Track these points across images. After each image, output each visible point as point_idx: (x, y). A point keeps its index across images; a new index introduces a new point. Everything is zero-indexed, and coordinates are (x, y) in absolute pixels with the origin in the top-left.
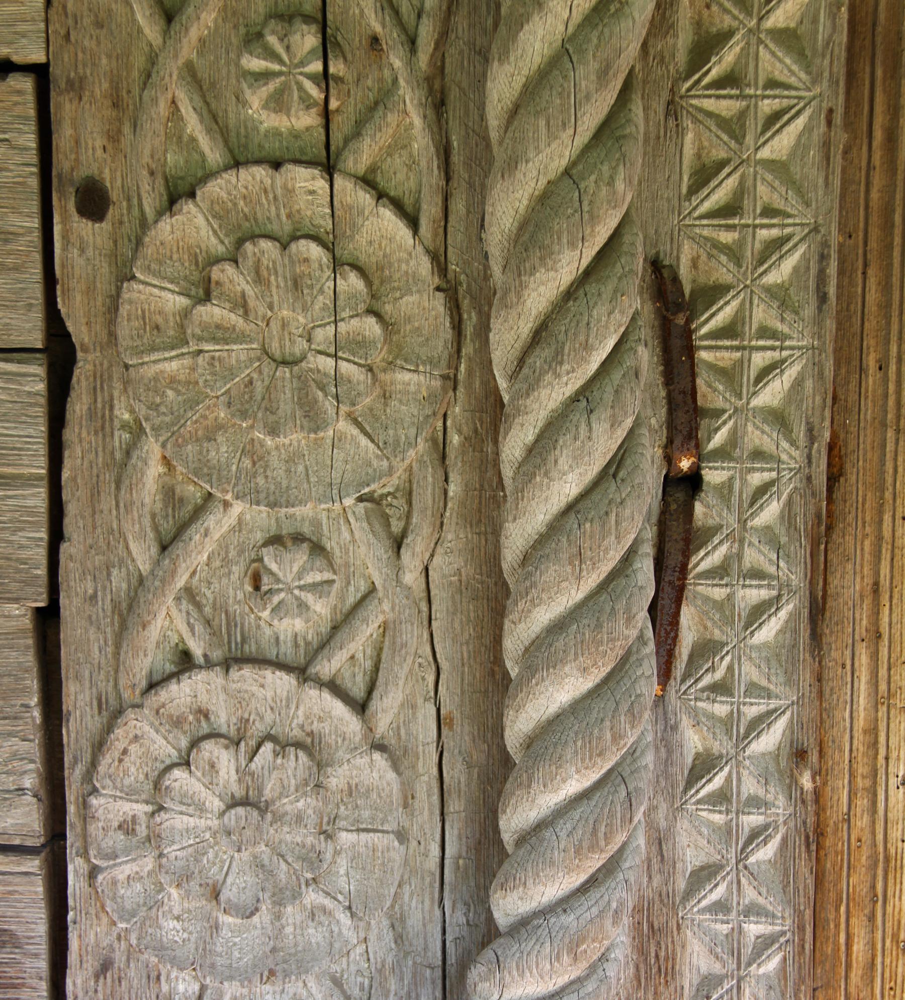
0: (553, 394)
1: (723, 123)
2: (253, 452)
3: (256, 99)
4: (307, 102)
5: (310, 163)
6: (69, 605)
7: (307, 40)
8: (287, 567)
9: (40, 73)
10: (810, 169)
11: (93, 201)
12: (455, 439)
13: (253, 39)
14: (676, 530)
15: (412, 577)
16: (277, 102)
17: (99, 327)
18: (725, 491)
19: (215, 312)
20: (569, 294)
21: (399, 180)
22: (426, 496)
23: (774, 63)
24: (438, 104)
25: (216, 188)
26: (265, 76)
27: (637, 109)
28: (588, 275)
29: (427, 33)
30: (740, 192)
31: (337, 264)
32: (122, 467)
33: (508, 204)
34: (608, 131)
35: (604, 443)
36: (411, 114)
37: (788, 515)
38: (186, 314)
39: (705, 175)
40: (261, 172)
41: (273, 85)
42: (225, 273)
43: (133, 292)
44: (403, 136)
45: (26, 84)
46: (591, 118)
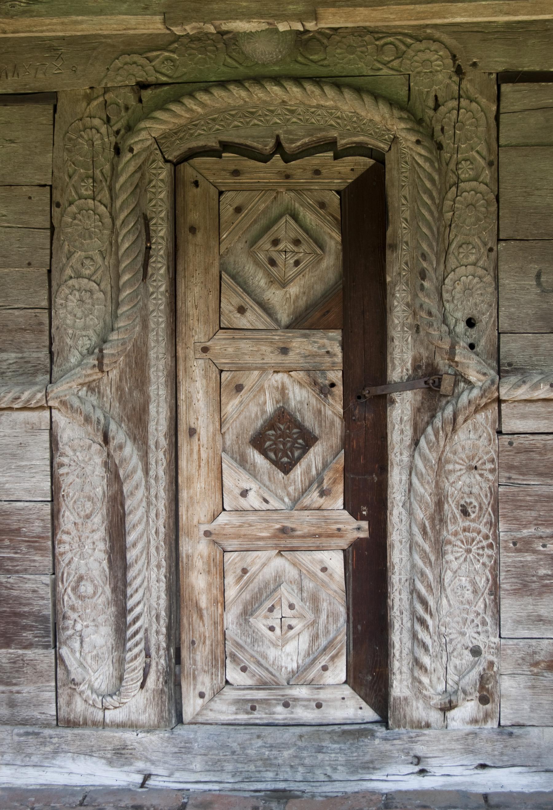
1: (153, 193)
2: (82, 244)
4: (90, 189)
7: (91, 181)
8: (87, 262)
10: (165, 200)
11: (58, 205)
13: (83, 181)
16: (86, 190)
18: (154, 249)
19: (76, 222)
20: (127, 216)
22: (109, 250)
23: (160, 184)
25: (77, 203)
29: (108, 180)
31: (95, 214)
32: (62, 246)
37: (164, 253)
39: (151, 200)
40: (83, 200)
43: (64, 219)
45: (48, 188)
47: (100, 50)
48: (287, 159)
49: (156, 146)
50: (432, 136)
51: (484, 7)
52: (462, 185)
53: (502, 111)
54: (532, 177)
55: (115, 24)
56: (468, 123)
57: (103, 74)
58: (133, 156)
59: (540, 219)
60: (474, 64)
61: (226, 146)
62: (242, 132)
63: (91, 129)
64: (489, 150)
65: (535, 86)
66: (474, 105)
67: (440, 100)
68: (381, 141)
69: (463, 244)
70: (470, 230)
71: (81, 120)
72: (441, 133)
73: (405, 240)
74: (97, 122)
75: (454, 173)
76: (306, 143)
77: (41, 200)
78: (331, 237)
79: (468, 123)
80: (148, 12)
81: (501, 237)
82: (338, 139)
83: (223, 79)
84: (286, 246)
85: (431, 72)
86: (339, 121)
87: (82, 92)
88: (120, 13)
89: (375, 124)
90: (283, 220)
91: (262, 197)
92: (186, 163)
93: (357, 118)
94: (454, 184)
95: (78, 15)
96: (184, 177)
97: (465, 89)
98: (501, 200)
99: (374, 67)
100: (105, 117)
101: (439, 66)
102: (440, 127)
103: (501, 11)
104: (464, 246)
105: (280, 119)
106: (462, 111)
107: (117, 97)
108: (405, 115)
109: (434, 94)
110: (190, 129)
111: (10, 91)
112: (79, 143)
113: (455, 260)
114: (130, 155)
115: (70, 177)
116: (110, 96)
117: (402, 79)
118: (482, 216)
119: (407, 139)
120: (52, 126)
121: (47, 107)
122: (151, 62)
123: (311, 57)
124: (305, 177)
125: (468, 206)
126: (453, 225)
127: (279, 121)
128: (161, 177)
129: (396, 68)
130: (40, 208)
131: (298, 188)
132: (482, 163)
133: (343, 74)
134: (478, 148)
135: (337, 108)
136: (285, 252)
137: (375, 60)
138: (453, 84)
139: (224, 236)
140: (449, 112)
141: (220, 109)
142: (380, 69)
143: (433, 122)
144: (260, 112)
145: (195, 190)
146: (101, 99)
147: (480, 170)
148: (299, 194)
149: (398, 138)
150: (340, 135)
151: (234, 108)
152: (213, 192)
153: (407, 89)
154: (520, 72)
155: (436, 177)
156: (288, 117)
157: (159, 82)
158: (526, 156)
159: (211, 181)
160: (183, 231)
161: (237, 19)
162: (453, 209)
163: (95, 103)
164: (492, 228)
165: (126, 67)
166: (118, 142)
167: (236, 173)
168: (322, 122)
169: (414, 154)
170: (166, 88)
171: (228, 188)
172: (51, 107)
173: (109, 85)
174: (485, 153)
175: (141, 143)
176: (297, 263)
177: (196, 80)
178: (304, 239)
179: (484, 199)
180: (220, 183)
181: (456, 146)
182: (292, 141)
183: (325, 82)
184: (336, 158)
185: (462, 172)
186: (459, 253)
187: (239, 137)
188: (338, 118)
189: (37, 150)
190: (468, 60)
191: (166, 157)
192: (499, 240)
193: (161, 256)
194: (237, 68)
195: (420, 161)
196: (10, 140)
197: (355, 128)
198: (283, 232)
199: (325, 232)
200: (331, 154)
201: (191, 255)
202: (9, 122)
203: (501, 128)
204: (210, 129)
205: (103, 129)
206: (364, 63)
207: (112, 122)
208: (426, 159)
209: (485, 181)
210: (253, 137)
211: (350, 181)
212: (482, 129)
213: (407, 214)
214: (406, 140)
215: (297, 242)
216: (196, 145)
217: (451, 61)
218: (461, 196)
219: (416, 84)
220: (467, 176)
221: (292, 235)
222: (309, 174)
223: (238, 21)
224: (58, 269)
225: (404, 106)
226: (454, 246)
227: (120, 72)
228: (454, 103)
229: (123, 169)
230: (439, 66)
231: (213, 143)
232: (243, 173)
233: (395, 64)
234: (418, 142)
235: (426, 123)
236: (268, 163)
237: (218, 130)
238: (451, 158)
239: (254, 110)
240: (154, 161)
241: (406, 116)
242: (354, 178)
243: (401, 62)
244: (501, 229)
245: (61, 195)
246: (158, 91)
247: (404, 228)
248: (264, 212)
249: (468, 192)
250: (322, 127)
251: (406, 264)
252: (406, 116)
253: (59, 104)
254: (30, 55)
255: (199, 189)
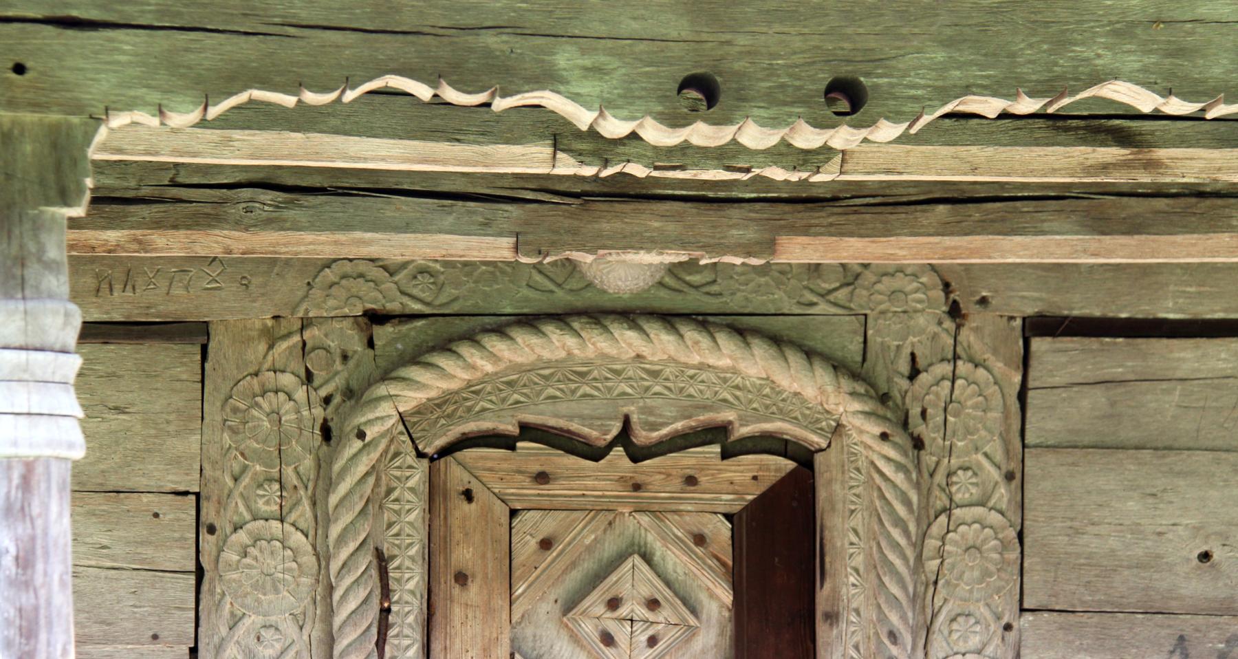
0: (348, 581)
1: (395, 511)
2: (258, 600)
3: (261, 502)
4: (276, 503)
6: (201, 646)
7: (276, 486)
8: (267, 635)
9: (198, 495)
10: (419, 524)
11: (212, 530)
12: (318, 598)
13: (260, 486)
14: (383, 623)
15: (306, 637)
16: (267, 503)
17: (212, 566)
18: (398, 613)
19: (248, 560)
20: (352, 554)
21: (302, 525)
22: (310, 613)
23: (409, 496)
24: (314, 504)
25: (248, 526)
27: (370, 506)
28: (357, 549)
29: (311, 486)
30: (400, 530)
31: (284, 547)
32: (219, 605)
33: (335, 531)
34: (363, 512)
35: (362, 593)
36: (306, 506)
37: (416, 619)
38: (239, 561)
39: (390, 525)
40: (262, 522)
42: (251, 550)
43: (223, 555)
44: (303, 513)
45: (193, 497)
46: (358, 508)
48: (637, 455)
49: (401, 427)
50: (905, 424)
51: (1058, 244)
52: (957, 512)
53: (1031, 384)
54: (1084, 502)
55: (429, 247)
56: (969, 403)
57: (300, 294)
58: (364, 446)
59: (1097, 576)
60: (983, 301)
61: (529, 431)
62: (563, 407)
63: (276, 392)
64: (1007, 452)
65: (1093, 343)
66: (981, 372)
67: (921, 363)
68: (814, 432)
69: (959, 615)
70: (971, 591)
71: (256, 375)
72: (921, 421)
73: (854, 605)
74: (287, 380)
75: (944, 490)
76: (677, 431)
77: (178, 520)
78: (712, 596)
79: (969, 403)
80: (490, 231)
81: (1026, 606)
82: (737, 425)
83: (526, 311)
84: (632, 611)
85: (905, 312)
86: (738, 393)
87: (258, 324)
88: (440, 232)
89: (804, 401)
90: (628, 565)
91: (589, 522)
92: (449, 458)
93: (772, 388)
94: (944, 510)
95: (366, 231)
96: (445, 483)
97: (965, 344)
98: (1027, 541)
99: (802, 300)
100: (303, 373)
101: (920, 301)
102: (919, 410)
103: (1085, 251)
104: (960, 619)
105: (632, 387)
106: (959, 382)
107: (326, 335)
108: (861, 388)
109: (909, 351)
110: (466, 399)
111: (117, 317)
112: (253, 417)
113: (944, 644)
114: (358, 444)
116: (312, 334)
117: (856, 324)
118: (992, 568)
119: (863, 429)
121: (189, 348)
122: (391, 275)
123: (688, 278)
124: (668, 489)
125: (968, 549)
126: (941, 583)
127: (629, 390)
128: (411, 483)
129: (841, 303)
130: (177, 535)
131: (656, 508)
132: (995, 475)
133: (747, 311)
134: (987, 449)
135: (735, 371)
136: (632, 620)
137: (806, 287)
138: (944, 335)
139: (520, 591)
140: (937, 384)
141: (522, 365)
142: (812, 304)
143: (908, 400)
144: (595, 374)
145: (465, 506)
146: (296, 339)
147: (990, 487)
148: (658, 518)
149: (844, 426)
150: (741, 418)
151: (548, 364)
152: (501, 511)
153: (861, 339)
154: (1066, 317)
155: (914, 498)
156: (646, 383)
157: (407, 311)
158: (1073, 464)
159: (496, 491)
160: (442, 581)
161: (642, 248)
162: (941, 554)
163: (283, 346)
164: (1010, 591)
165: (344, 282)
166: (329, 418)
167: (542, 478)
168: (708, 394)
169: (875, 458)
170: (420, 323)
171: (525, 505)
172: (197, 349)
173: (311, 315)
174: (999, 456)
175: (379, 422)
176: (652, 641)
177: (477, 311)
178: (665, 598)
179: (996, 538)
180: (513, 494)
181: (948, 443)
182: (654, 427)
183: (715, 324)
184: (725, 455)
185: (959, 490)
186: (951, 632)
187: (556, 416)
188: (737, 387)
189: (171, 428)
190: (972, 294)
191: (420, 447)
192: (1022, 610)
193: (410, 625)
194: (552, 292)
195: (888, 470)
196: (116, 408)
197: (767, 407)
198: (628, 585)
199: (700, 586)
200: (716, 449)
201: (457, 623)
202: (113, 375)
203: (1029, 414)
204: (504, 400)
205: (300, 394)
206: (785, 292)
207: (316, 383)
208: (899, 467)
209: (998, 507)
210: (582, 417)
211: (750, 497)
212: (995, 415)
213: (859, 561)
214: (861, 432)
215: (653, 604)
216: (475, 429)
217: (942, 294)
218: (955, 531)
219: (878, 332)
220: (967, 495)
221: (645, 591)
222: (677, 483)
223: (642, 252)
224: (211, 646)
225: (853, 371)
226: (941, 618)
227: (334, 290)
228: (947, 368)
229: (344, 471)
230: (920, 301)
231: (509, 427)
232: (556, 479)
233: (841, 295)
234: (884, 437)
235: (895, 402)
236: (602, 462)
237: (518, 402)
238: (938, 463)
239: (585, 369)
240: (396, 454)
241: (862, 391)
242: (758, 493)
243: (852, 293)
244: (1026, 591)
246: (405, 328)
247: (854, 585)
248: (589, 549)
249: (969, 525)
250: (709, 403)
251: (857, 647)
252: (862, 391)
253: (212, 346)
255: (473, 505)
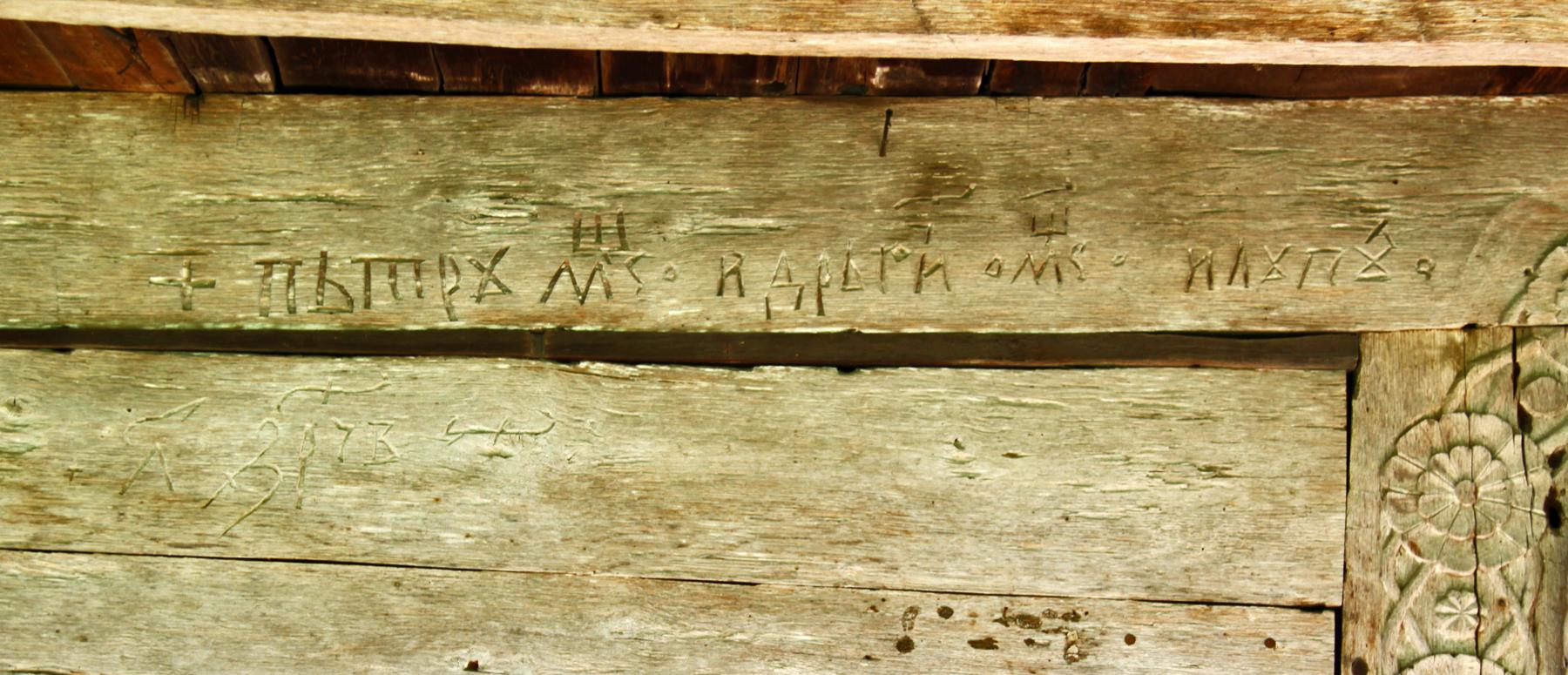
4: (1469, 627)
5: (1471, 654)
7: (1470, 599)
9: (1338, 611)
16: (1455, 626)
26: (1450, 615)
29: (1529, 599)
40: (1447, 658)
41: (1453, 619)
45: (1332, 615)
47: (1507, 217)
74: (1488, 427)
87: (1440, 339)
107: (1555, 355)
111: (1218, 324)
112: (1431, 486)
115: (1403, 586)
116: (1532, 354)
120: (1344, 434)
121: (1327, 376)
163: (1484, 371)
166: (1559, 488)
172: (1340, 378)
173: (1531, 322)
189: (1298, 502)
196: (1209, 469)
205: (1511, 450)
207: (1538, 431)
245: (1371, 641)
253: (1365, 370)
254: (1286, 223)
